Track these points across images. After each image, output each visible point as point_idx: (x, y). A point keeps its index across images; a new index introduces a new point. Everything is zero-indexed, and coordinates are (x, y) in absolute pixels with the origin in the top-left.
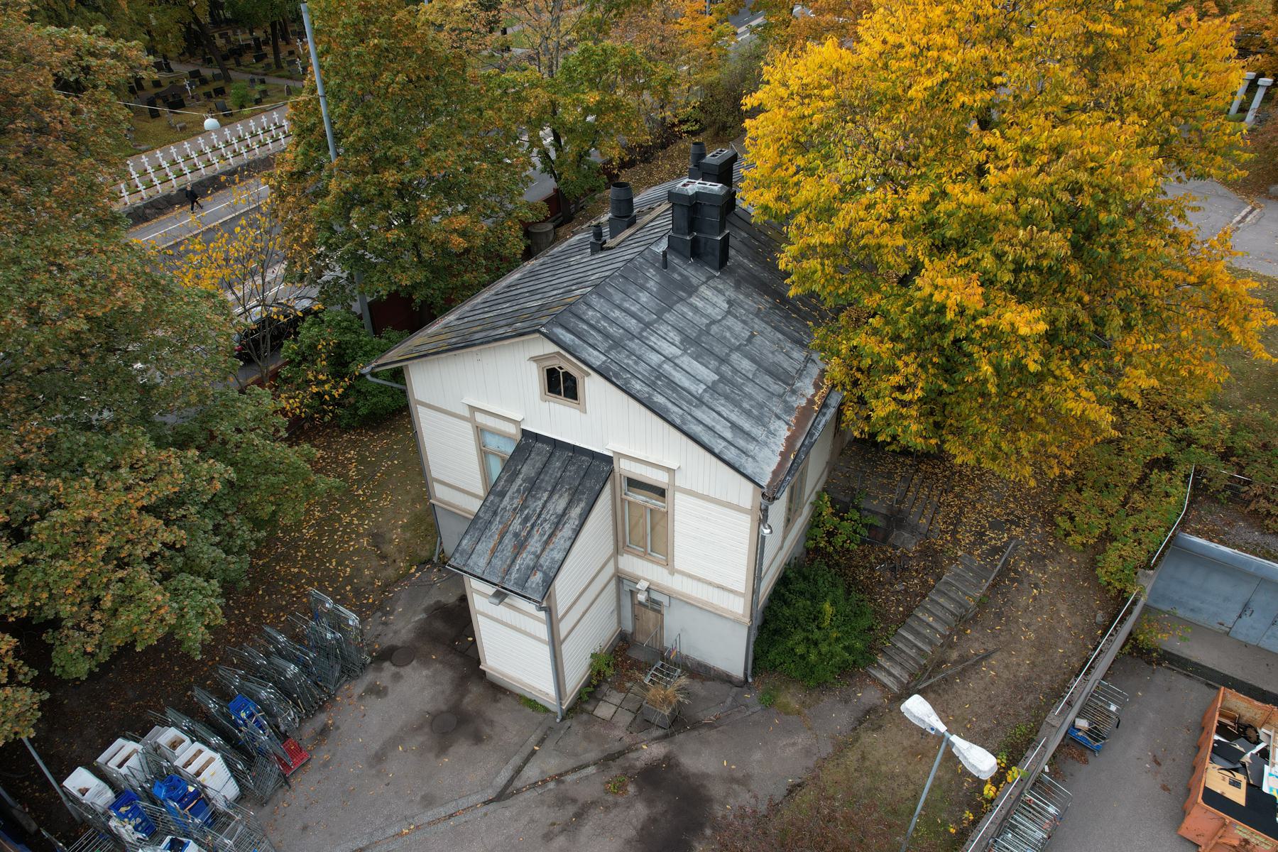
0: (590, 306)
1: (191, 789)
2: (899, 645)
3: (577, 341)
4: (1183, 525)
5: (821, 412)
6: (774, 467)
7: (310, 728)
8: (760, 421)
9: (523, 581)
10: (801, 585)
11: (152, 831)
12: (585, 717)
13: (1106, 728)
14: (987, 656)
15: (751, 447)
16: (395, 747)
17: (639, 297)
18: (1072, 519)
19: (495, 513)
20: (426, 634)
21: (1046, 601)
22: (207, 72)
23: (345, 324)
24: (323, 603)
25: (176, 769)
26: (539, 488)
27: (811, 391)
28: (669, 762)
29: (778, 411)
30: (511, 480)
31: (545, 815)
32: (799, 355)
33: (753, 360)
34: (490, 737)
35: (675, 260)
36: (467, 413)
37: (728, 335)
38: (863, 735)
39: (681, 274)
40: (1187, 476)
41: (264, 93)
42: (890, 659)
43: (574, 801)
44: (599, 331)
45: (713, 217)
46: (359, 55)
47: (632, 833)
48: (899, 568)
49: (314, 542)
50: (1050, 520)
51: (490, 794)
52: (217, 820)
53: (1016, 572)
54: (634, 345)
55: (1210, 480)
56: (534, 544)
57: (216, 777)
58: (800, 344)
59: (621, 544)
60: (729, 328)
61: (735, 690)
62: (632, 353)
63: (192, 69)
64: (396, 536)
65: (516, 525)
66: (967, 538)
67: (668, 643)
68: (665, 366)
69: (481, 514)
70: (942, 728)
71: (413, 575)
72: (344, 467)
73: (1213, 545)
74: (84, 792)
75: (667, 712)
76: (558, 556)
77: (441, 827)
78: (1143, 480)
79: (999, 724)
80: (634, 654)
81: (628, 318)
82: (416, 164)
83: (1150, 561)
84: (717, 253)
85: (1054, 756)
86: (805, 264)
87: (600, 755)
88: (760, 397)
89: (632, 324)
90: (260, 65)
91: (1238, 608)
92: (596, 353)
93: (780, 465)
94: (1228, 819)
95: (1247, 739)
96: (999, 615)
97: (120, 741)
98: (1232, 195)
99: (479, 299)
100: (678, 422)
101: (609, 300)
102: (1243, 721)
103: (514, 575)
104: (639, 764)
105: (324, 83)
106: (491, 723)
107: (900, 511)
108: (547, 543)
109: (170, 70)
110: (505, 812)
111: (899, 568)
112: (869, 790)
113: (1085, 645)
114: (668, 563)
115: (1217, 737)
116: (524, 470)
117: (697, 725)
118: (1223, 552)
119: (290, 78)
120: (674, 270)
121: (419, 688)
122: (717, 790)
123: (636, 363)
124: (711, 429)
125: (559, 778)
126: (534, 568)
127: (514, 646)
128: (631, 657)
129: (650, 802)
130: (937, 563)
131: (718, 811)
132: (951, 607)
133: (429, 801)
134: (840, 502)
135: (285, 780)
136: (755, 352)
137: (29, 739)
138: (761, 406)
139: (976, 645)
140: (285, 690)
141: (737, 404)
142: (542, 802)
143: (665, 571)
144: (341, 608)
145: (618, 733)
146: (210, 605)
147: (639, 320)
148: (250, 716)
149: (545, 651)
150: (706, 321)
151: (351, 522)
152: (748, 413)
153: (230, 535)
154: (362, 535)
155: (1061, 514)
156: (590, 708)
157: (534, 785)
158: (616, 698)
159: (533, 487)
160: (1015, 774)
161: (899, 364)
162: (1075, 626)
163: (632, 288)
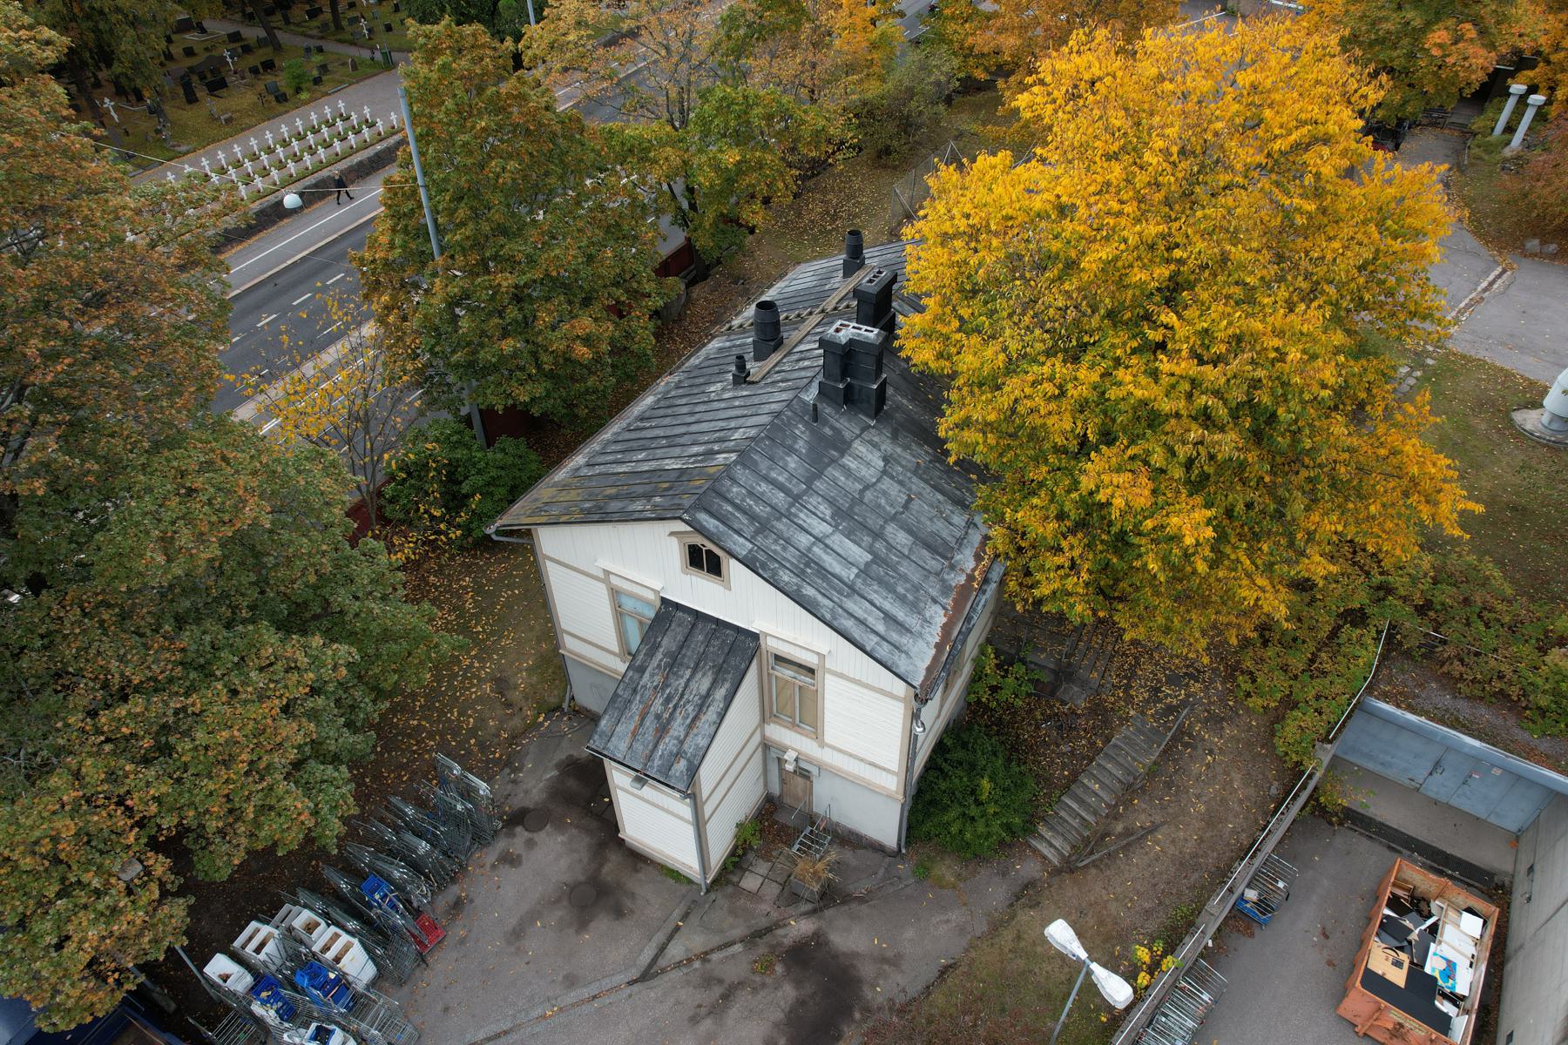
0: (734, 481)
1: (332, 976)
2: (1062, 814)
3: (722, 527)
4: (1370, 690)
5: (982, 591)
6: (928, 662)
7: (444, 901)
8: (915, 607)
9: (667, 768)
10: (959, 754)
11: (289, 1014)
12: (730, 889)
13: (1275, 900)
14: (1153, 829)
15: (904, 640)
16: (533, 921)
17: (786, 463)
18: (1254, 681)
19: (635, 691)
20: (558, 794)
21: (1219, 770)
22: (253, 33)
23: (454, 438)
24: (451, 770)
25: (314, 954)
26: (681, 664)
27: (971, 564)
28: (818, 939)
29: (934, 593)
30: (651, 654)
31: (692, 997)
32: (959, 519)
33: (910, 532)
34: (632, 911)
35: (827, 410)
36: (601, 575)
37: (883, 501)
38: (1020, 912)
39: (832, 428)
40: (1379, 632)
41: (324, 68)
42: (1052, 828)
43: (720, 981)
44: (744, 512)
45: (868, 364)
46: (465, 144)
47: (779, 1015)
48: (1065, 726)
49: (433, 689)
50: (1230, 676)
51: (634, 973)
52: (358, 1004)
53: (1190, 735)
54: (780, 526)
55: (1405, 637)
56: (677, 728)
57: (357, 964)
58: (962, 504)
59: (767, 715)
60: (885, 493)
61: (888, 860)
62: (780, 537)
63: (232, 29)
64: (522, 680)
65: (657, 706)
66: (1141, 695)
67: (819, 808)
68: (815, 549)
69: (620, 692)
70: (1083, 955)
71: (541, 724)
72: (460, 597)
73: (1399, 712)
74: (225, 978)
75: (816, 888)
76: (703, 743)
77: (586, 1008)
78: (1334, 634)
79: (1160, 903)
80: (781, 818)
81: (776, 491)
82: (532, 261)
83: (1329, 733)
84: (873, 402)
85: (1219, 929)
86: (966, 433)
87: (747, 932)
88: (915, 577)
89: (780, 498)
90: (315, 23)
91: (1430, 766)
92: (741, 540)
93: (935, 659)
94: (1384, 1003)
95: (1420, 912)
96: (1168, 785)
97: (254, 924)
98: (1484, 251)
99: (607, 435)
100: (828, 617)
101: (756, 472)
102: (1418, 893)
103: (657, 762)
104: (787, 942)
105: (422, 154)
106: (633, 896)
107: (1069, 664)
108: (690, 727)
109: (203, 31)
110: (650, 992)
111: (1065, 726)
112: (1023, 973)
113: (1256, 820)
114: (816, 733)
115: (1387, 912)
116: (665, 642)
117: (847, 899)
118: (1408, 721)
119: (353, 43)
120: (826, 422)
121: (553, 856)
122: (866, 970)
123: (784, 549)
124: (862, 622)
125: (704, 956)
126: (678, 755)
127: (653, 821)
128: (781, 822)
129: (798, 983)
130: (1106, 723)
131: (868, 993)
132: (1119, 773)
133: (571, 981)
134: (1004, 653)
135: (422, 959)
136: (912, 521)
137: (182, 947)
138: (916, 588)
139: (1143, 817)
140: (416, 867)
141: (891, 589)
142: (688, 983)
143: (815, 744)
144: (471, 776)
145: (765, 907)
146: (343, 796)
147: (787, 492)
148: (384, 897)
149: (690, 831)
150: (859, 487)
151: (471, 666)
152: (902, 599)
153: (352, 707)
154: (484, 681)
155: (1242, 673)
156: (735, 879)
157: (679, 965)
158: (762, 867)
159: (674, 663)
160: (1169, 963)
161: (1064, 544)
162: (1248, 798)
163: (780, 452)
